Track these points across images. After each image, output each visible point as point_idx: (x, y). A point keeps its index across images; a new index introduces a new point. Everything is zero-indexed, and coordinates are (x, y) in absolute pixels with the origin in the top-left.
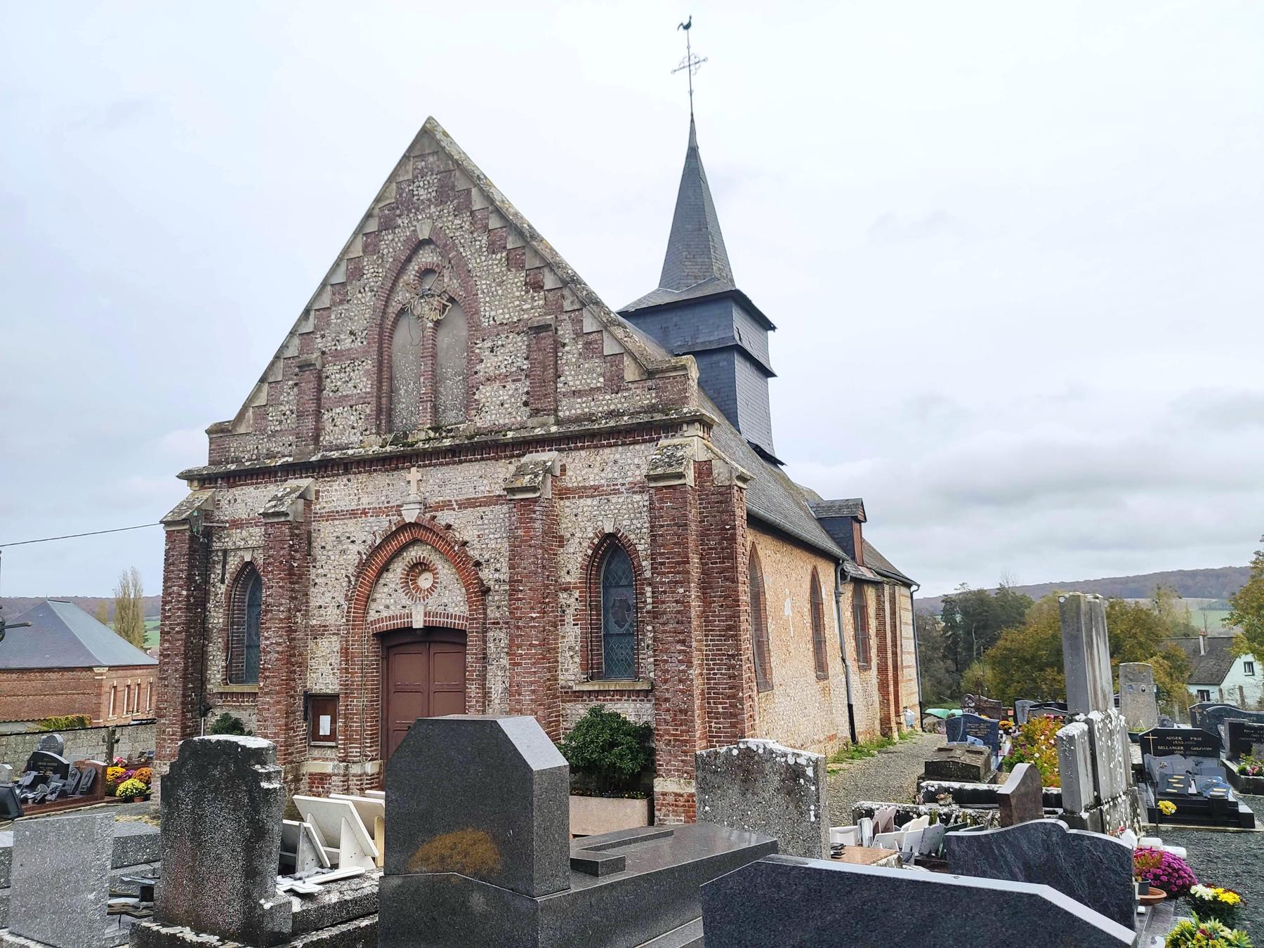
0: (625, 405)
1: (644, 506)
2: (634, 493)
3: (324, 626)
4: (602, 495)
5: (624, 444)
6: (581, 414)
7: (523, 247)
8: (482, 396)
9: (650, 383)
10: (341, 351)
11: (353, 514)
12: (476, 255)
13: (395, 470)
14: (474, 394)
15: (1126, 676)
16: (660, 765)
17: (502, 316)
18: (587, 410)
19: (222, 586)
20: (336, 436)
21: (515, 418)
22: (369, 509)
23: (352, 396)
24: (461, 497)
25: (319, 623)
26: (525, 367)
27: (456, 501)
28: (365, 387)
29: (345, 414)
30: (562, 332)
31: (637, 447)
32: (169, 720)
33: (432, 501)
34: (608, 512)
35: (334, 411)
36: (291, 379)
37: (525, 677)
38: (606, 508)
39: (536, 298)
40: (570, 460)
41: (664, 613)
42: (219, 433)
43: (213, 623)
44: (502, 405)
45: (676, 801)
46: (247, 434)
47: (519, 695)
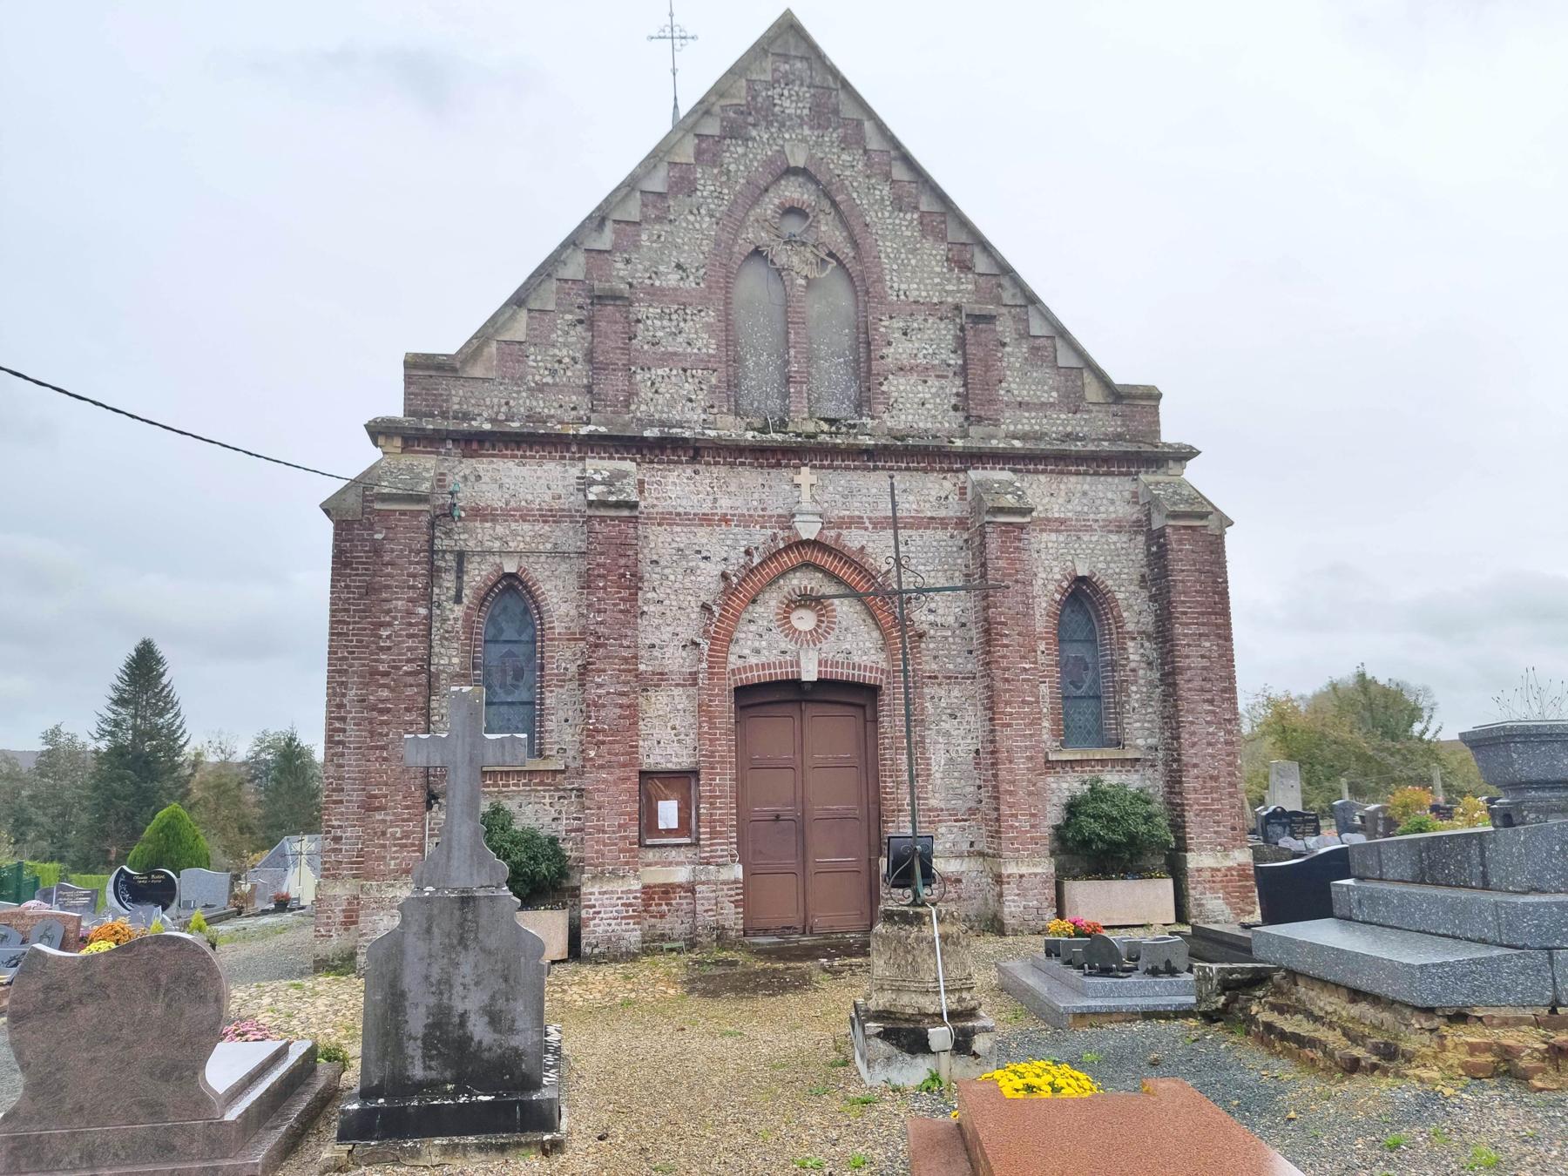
0: (1085, 429)
1: (1122, 548)
2: (1110, 532)
3: (662, 674)
4: (1070, 531)
5: (1096, 474)
6: (1029, 431)
7: (943, 214)
8: (893, 389)
9: (1114, 408)
10: (661, 289)
11: (705, 520)
12: (876, 207)
13: (773, 467)
14: (881, 384)
15: (1278, 773)
16: (1191, 838)
17: (917, 293)
18: (1037, 428)
19: (456, 608)
20: (659, 408)
21: (940, 423)
22: (734, 515)
23: (685, 355)
24: (877, 514)
25: (650, 668)
26: (952, 362)
27: (870, 518)
28: (707, 346)
29: (673, 378)
30: (1001, 329)
31: (1110, 479)
32: (394, 814)
33: (836, 513)
34: (1078, 552)
35: (653, 371)
36: (571, 312)
37: (1017, 741)
38: (1076, 546)
39: (963, 280)
40: (1026, 484)
41: (1189, 668)
42: (421, 369)
43: (438, 664)
44: (923, 404)
45: (1213, 876)
46: (484, 380)
47: (1011, 762)
